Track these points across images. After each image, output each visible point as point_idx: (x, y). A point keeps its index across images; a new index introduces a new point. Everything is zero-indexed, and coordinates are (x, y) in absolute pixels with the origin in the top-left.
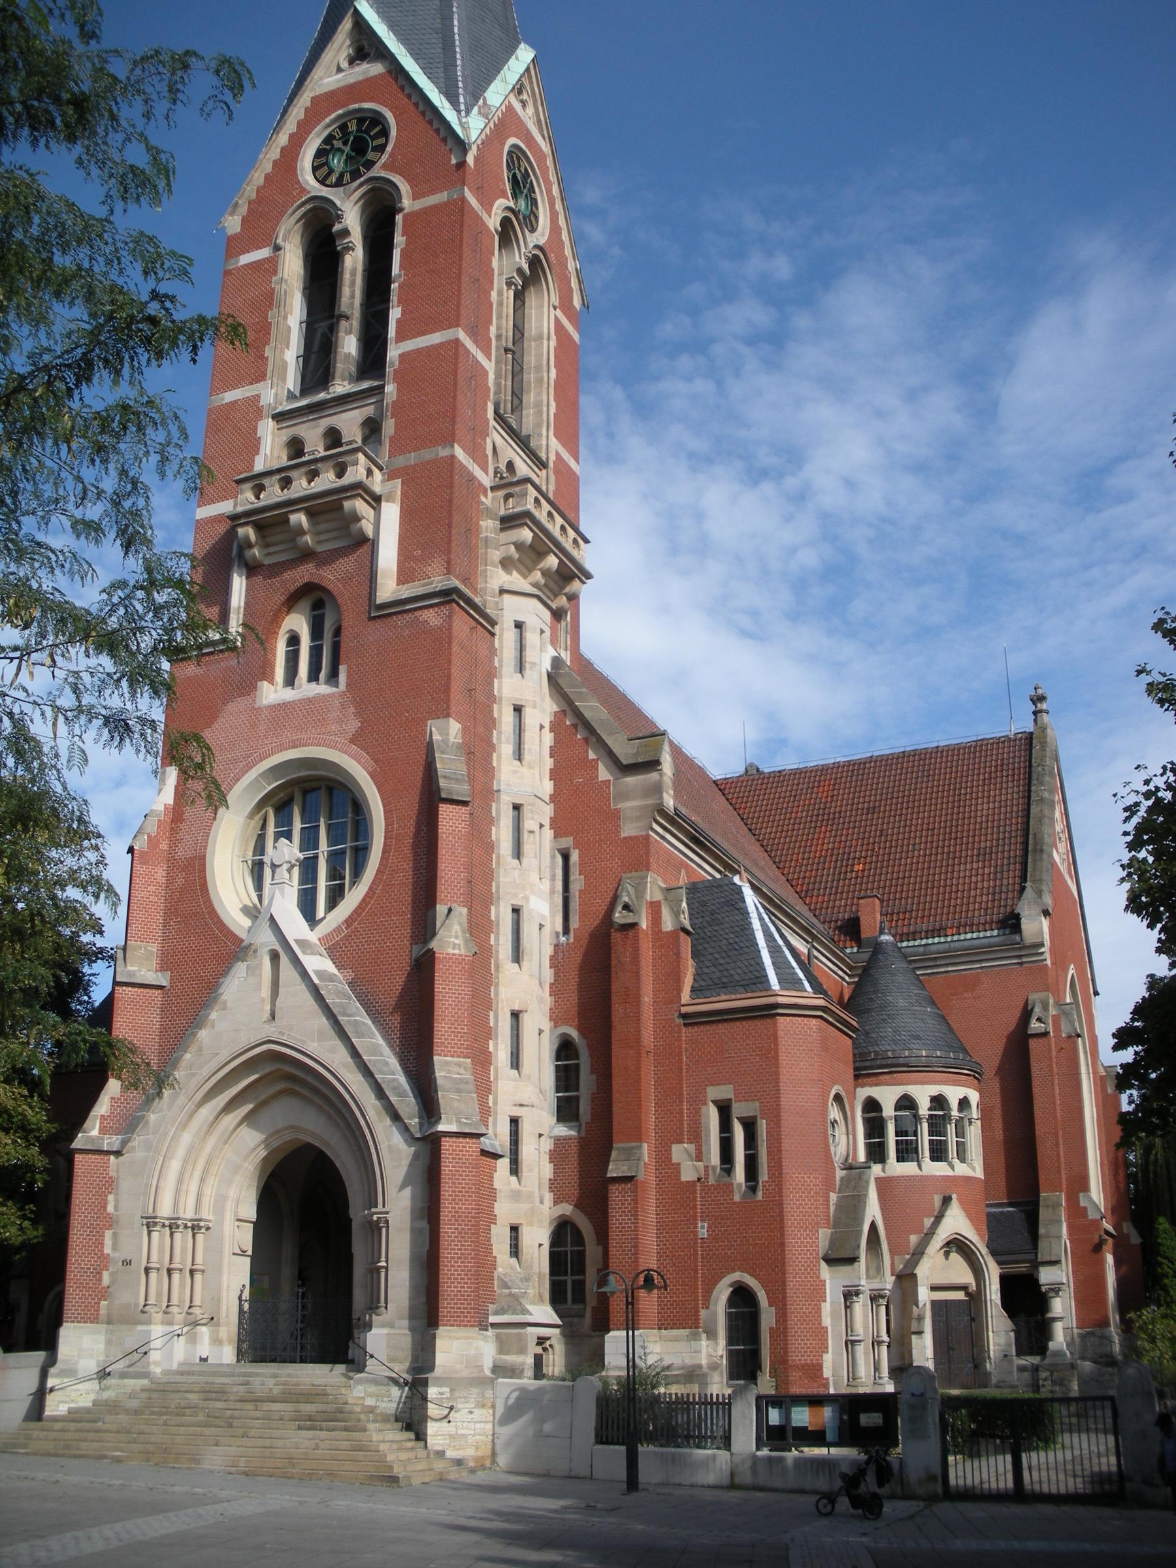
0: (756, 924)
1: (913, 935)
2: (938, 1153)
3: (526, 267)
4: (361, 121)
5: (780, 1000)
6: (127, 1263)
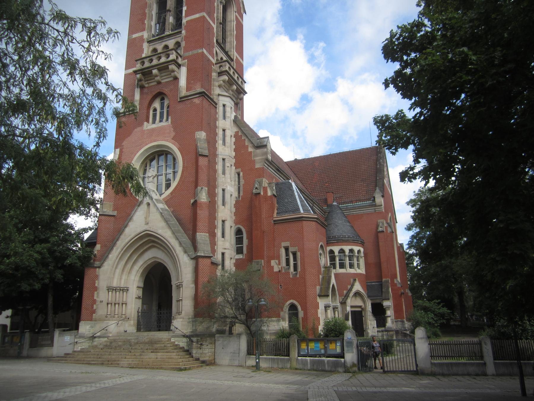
0: (296, 194)
1: (344, 203)
2: (351, 266)
5: (303, 215)
6: (101, 302)
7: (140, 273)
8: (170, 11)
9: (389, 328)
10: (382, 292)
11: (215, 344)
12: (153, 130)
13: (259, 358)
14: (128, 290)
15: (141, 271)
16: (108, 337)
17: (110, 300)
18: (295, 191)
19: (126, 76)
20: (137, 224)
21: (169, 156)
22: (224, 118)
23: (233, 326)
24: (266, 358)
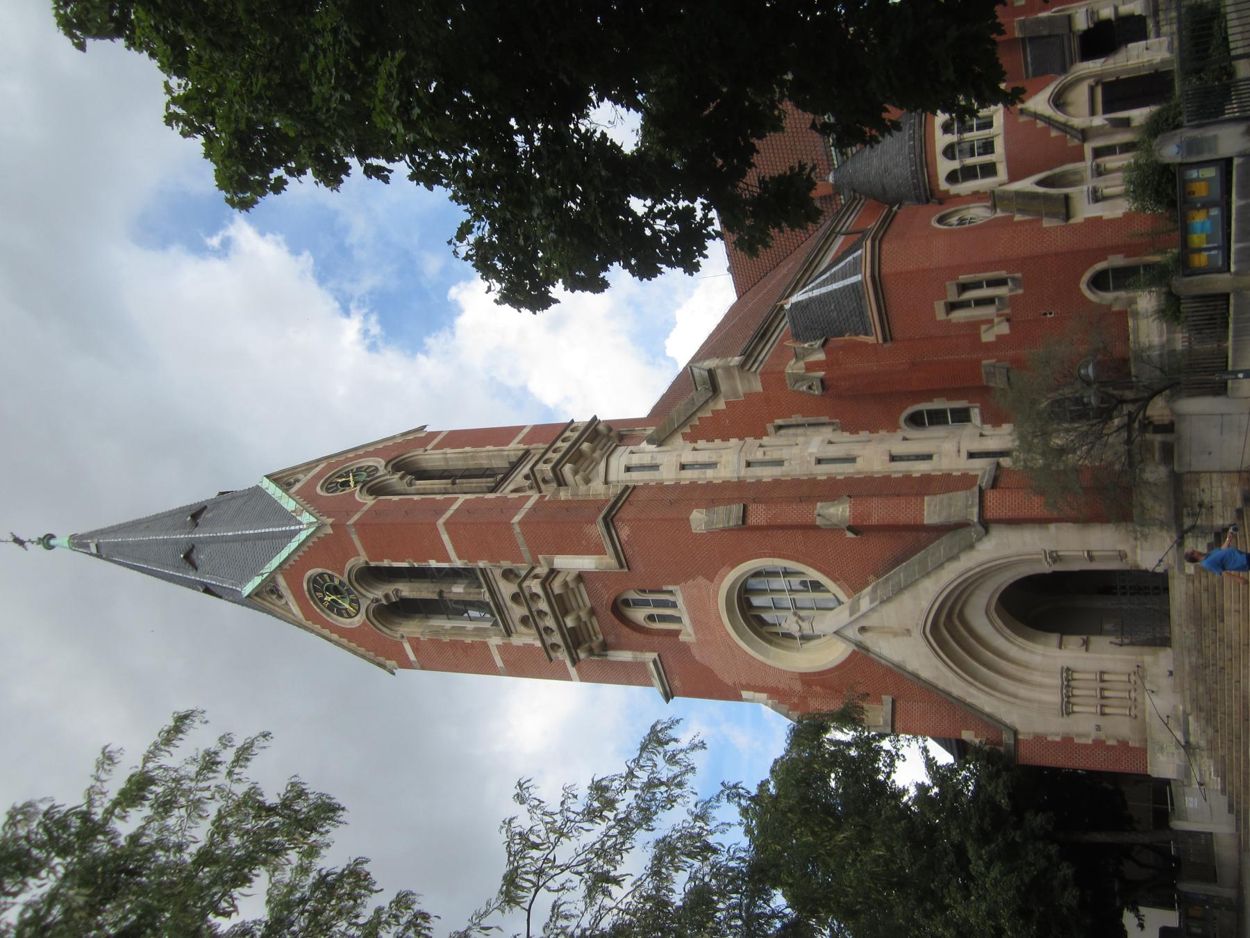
0: (816, 292)
3: (399, 474)
4: (316, 590)
5: (868, 274)
6: (1098, 728)
7: (1025, 642)
8: (441, 593)
9: (1147, 7)
10: (1050, 36)
11: (1198, 473)
12: (695, 622)
13: (1235, 373)
14: (1068, 669)
15: (1020, 640)
16: (1186, 715)
17: (1093, 710)
18: (810, 294)
19: (583, 678)
20: (914, 655)
21: (749, 586)
22: (655, 467)
23: (1151, 423)
24: (1235, 341)
